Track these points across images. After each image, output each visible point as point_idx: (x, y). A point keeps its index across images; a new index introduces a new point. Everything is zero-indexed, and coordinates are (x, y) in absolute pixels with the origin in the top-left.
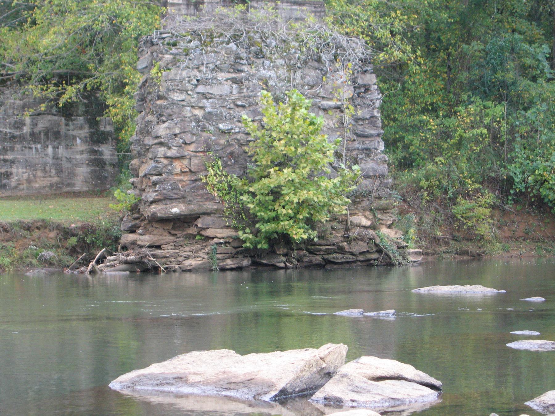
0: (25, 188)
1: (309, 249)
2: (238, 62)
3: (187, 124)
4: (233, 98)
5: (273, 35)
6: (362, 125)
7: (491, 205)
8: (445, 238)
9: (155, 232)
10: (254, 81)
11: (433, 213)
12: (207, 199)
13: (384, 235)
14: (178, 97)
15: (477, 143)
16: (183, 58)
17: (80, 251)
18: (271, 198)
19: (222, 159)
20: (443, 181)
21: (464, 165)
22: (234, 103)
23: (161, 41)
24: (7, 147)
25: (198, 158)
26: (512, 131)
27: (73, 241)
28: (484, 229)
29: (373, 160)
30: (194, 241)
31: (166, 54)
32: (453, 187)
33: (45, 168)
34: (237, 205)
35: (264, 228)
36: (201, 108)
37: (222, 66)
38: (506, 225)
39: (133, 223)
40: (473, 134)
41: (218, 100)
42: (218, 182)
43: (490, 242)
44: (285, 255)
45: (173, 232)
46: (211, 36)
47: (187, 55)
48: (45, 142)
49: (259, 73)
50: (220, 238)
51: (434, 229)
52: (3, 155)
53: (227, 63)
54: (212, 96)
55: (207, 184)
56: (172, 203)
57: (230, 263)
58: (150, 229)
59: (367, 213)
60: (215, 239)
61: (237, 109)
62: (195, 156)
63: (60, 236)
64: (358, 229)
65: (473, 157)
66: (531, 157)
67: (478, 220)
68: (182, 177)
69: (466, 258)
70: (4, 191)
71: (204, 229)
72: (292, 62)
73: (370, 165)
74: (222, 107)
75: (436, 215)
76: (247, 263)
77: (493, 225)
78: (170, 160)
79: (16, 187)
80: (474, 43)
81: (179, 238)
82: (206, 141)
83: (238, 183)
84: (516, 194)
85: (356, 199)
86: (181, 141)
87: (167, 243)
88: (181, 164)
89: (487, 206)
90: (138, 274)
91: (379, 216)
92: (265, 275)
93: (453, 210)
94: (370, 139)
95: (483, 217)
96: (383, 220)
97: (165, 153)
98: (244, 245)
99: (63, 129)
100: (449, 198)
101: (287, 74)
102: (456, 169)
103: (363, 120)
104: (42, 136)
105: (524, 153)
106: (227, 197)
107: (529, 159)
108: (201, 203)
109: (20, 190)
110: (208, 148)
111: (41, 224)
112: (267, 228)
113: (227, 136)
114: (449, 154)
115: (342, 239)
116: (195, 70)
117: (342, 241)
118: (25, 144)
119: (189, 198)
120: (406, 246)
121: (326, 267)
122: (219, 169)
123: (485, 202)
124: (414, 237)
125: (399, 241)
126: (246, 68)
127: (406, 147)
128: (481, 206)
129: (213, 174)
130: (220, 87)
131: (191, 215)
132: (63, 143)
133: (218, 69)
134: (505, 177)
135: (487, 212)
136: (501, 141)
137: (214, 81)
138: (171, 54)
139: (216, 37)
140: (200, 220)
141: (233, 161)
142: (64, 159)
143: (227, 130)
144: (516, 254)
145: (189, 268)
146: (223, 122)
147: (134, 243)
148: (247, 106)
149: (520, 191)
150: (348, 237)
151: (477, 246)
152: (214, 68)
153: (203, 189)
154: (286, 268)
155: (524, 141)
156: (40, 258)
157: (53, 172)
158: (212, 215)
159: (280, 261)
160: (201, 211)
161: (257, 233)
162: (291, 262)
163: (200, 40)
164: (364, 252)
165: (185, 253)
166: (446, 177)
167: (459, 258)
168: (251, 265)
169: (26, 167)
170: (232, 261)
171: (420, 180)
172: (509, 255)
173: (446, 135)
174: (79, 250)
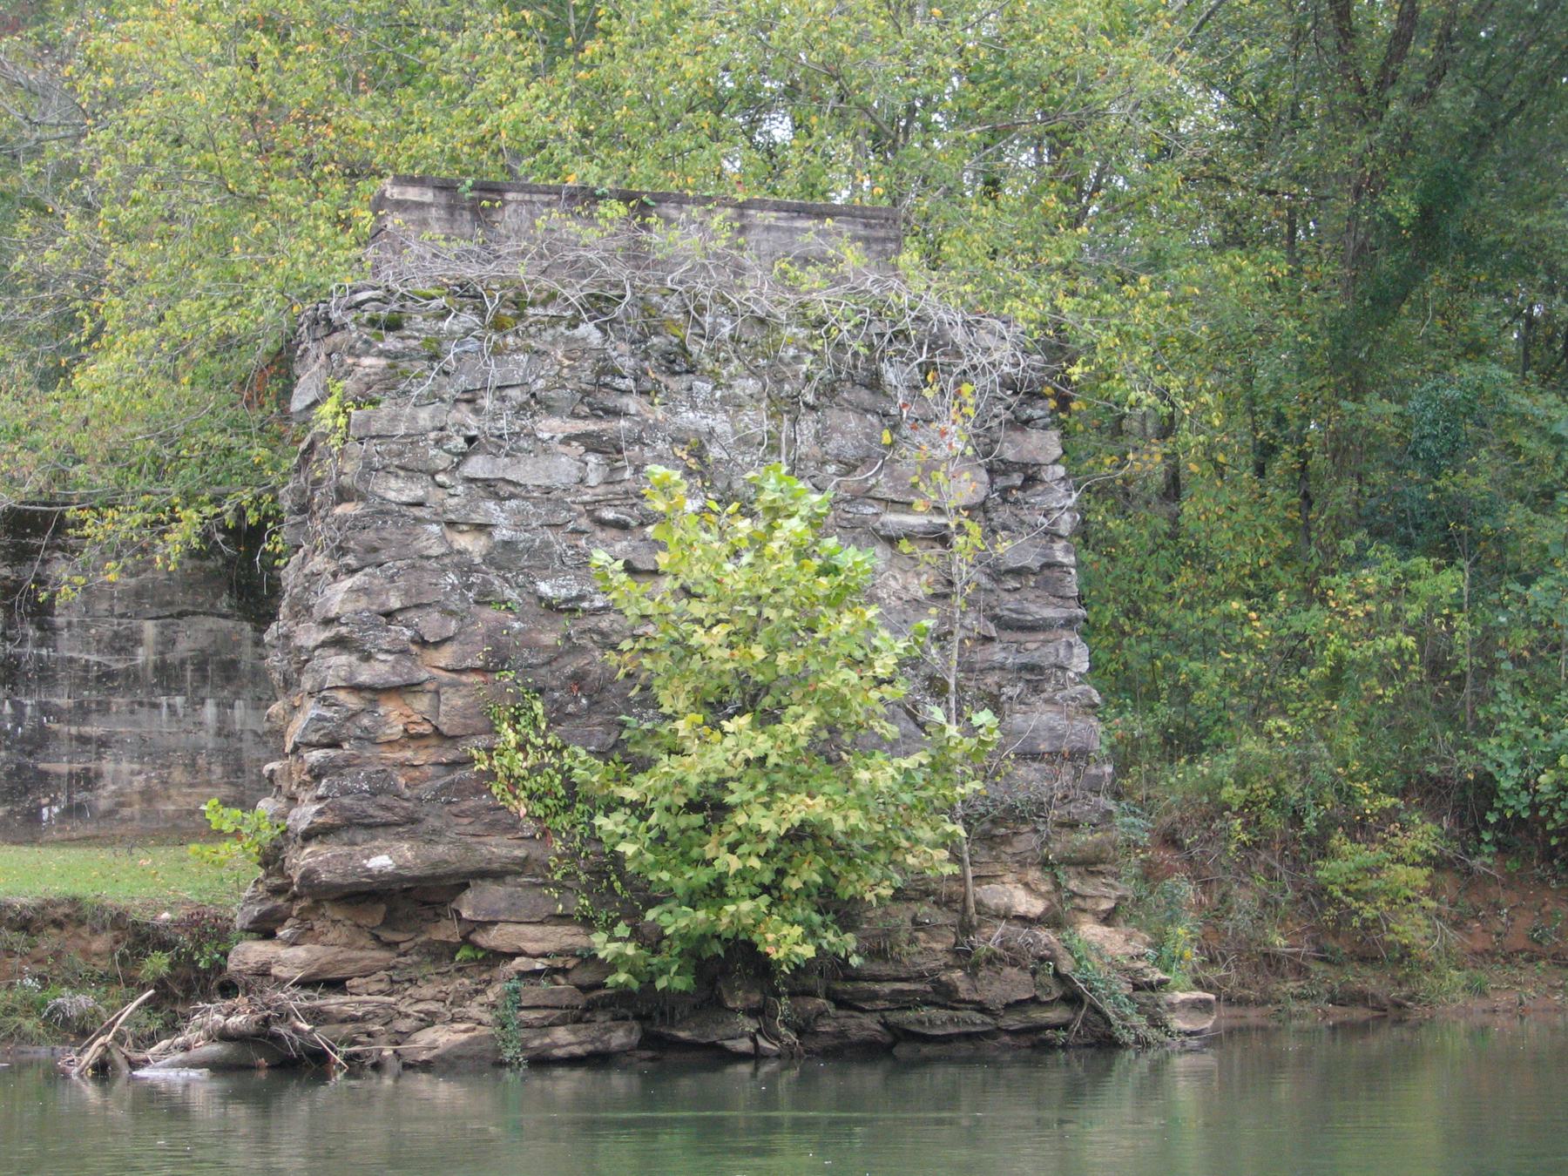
0: (138, 816)
1: (835, 992)
2: (606, 385)
3: (428, 578)
4: (586, 498)
5: (725, 302)
6: (1016, 589)
7: (1430, 857)
8: (1296, 955)
9: (331, 936)
10: (660, 446)
11: (1260, 881)
12: (492, 827)
13: (1089, 943)
14: (400, 491)
15: (1387, 677)
16: (420, 366)
17: (181, 994)
18: (697, 819)
19: (548, 694)
20: (1288, 789)
21: (1350, 742)
22: (590, 513)
23: (353, 314)
24: (90, 702)
25: (464, 691)
26: (1484, 644)
27: (158, 963)
28: (1411, 930)
29: (1048, 701)
30: (452, 967)
31: (367, 353)
32: (1317, 805)
33: (194, 760)
34: (594, 847)
35: (674, 920)
36: (481, 528)
37: (551, 394)
38: (1476, 917)
39: (268, 905)
40: (1376, 651)
41: (534, 505)
42: (531, 770)
43: (1429, 967)
44: (752, 1013)
45: (388, 936)
46: (519, 303)
47: (434, 357)
48: (195, 690)
49: (677, 419)
50: (535, 957)
51: (1262, 928)
52: (79, 725)
53: (569, 385)
54: (517, 490)
55: (491, 775)
56: (374, 838)
57: (564, 1039)
58: (318, 925)
59: (1033, 874)
60: (518, 960)
61: (600, 535)
62: (454, 685)
63: (122, 948)
64: (1002, 926)
65: (1375, 720)
66: (1544, 719)
67: (1393, 902)
68: (409, 754)
69: (1359, 1014)
70: (76, 823)
71: (484, 925)
72: (787, 387)
73: (1039, 719)
74: (549, 526)
75: (1270, 887)
76: (624, 1040)
77: (1438, 916)
78: (368, 695)
79: (111, 813)
80: (1371, 397)
81: (405, 954)
82: (490, 636)
83: (588, 771)
84: (1502, 824)
85: (992, 829)
86: (409, 633)
87: (366, 973)
88: (410, 712)
89: (1419, 859)
90: (262, 1075)
91: (1073, 885)
92: (686, 1084)
93: (1318, 873)
94: (1041, 637)
95: (1410, 893)
96: (1084, 897)
97: (352, 673)
98: (610, 980)
99: (247, 655)
100: (1308, 839)
101: (767, 425)
102: (1326, 754)
103: (1019, 572)
104: (189, 674)
105: (1524, 707)
106: (563, 821)
107: (1540, 724)
108: (470, 840)
109: (123, 821)
110: (498, 660)
111: (67, 911)
112: (682, 923)
113: (565, 621)
114: (1306, 712)
115: (949, 959)
116: (464, 407)
117: (948, 967)
118: (140, 694)
119: (433, 822)
120: (1162, 983)
121: (895, 1051)
122: (536, 727)
123: (1413, 848)
124: (1188, 953)
125: (1139, 965)
126: (632, 404)
127: (1184, 693)
128: (1400, 860)
129: (513, 744)
130: (544, 462)
131: (433, 878)
132: (247, 694)
133: (540, 404)
134: (1471, 777)
135: (1420, 876)
136: (1455, 672)
137: (524, 444)
138: (381, 354)
139: (532, 304)
140: (469, 895)
141: (584, 701)
142: (248, 736)
143: (567, 601)
144: (1509, 1002)
145: (424, 1056)
146: (555, 574)
147: (263, 972)
148: (633, 523)
149: (1516, 816)
150: (968, 954)
151: (1393, 978)
152: (527, 403)
153: (478, 792)
154: (756, 1056)
155: (1523, 674)
156: (51, 1014)
157: (218, 770)
158: (509, 879)
159: (740, 1033)
160: (469, 866)
161: (652, 940)
162: (777, 1037)
163: (482, 313)
164: (1020, 1003)
165: (421, 1006)
166: (1298, 776)
167: (1339, 1014)
168: (642, 1045)
169: (141, 757)
170: (574, 1033)
171: (1222, 785)
172: (1485, 1004)
173: (1297, 655)
174: (178, 991)
